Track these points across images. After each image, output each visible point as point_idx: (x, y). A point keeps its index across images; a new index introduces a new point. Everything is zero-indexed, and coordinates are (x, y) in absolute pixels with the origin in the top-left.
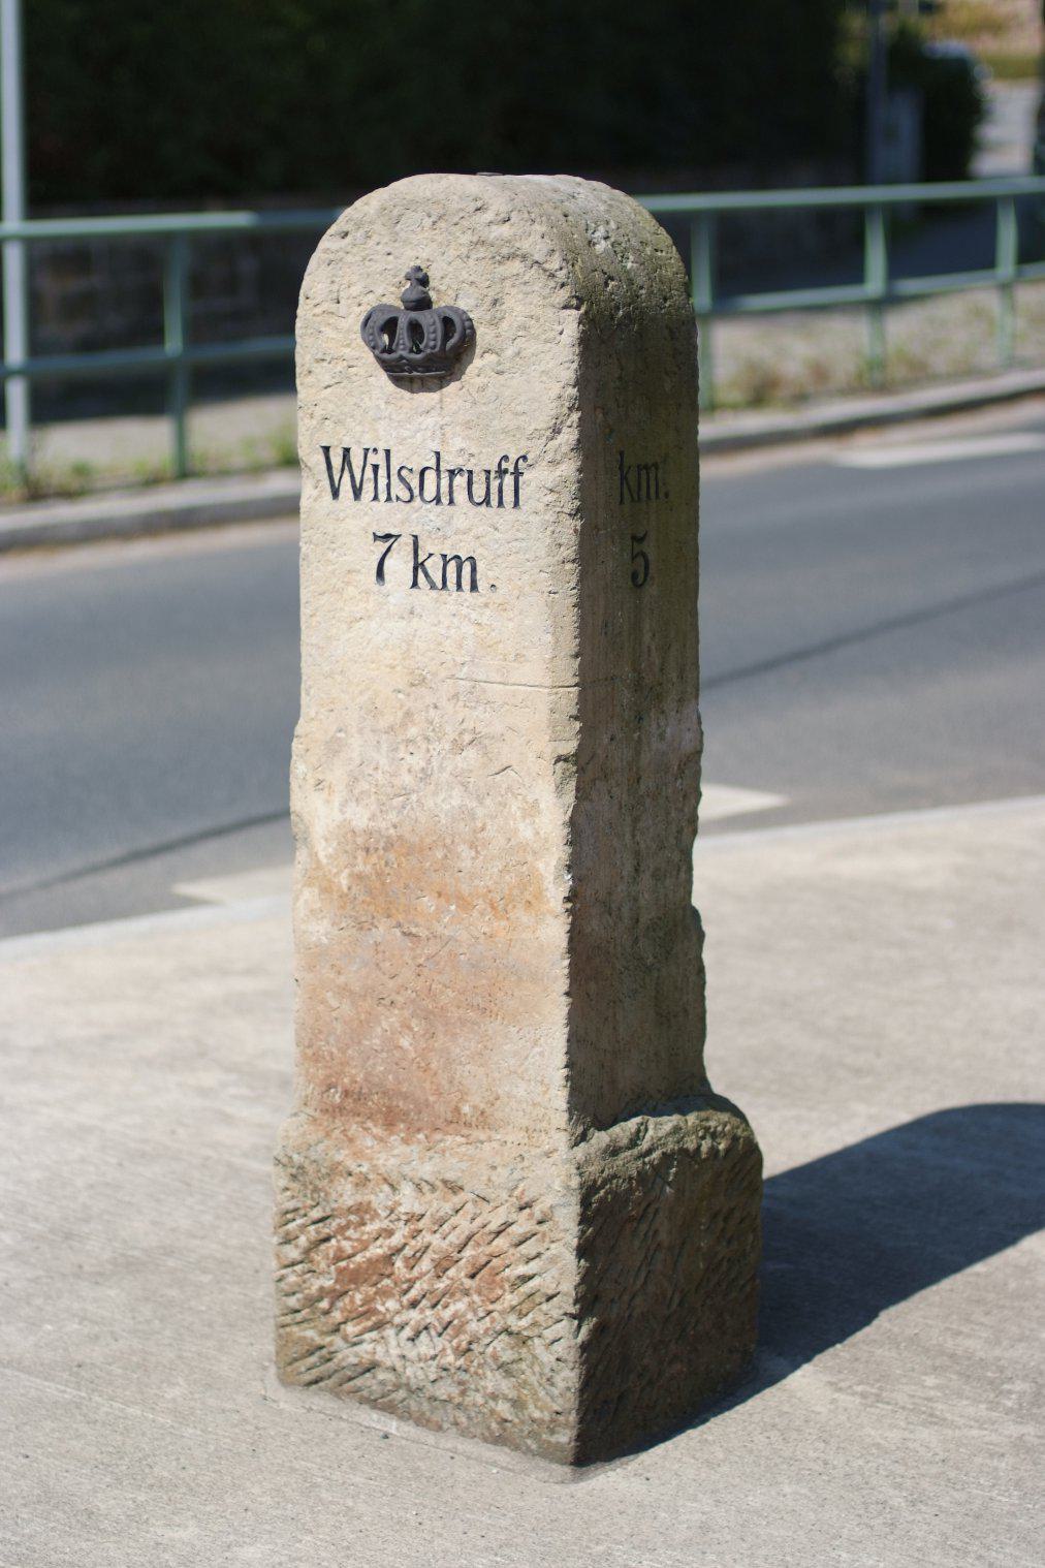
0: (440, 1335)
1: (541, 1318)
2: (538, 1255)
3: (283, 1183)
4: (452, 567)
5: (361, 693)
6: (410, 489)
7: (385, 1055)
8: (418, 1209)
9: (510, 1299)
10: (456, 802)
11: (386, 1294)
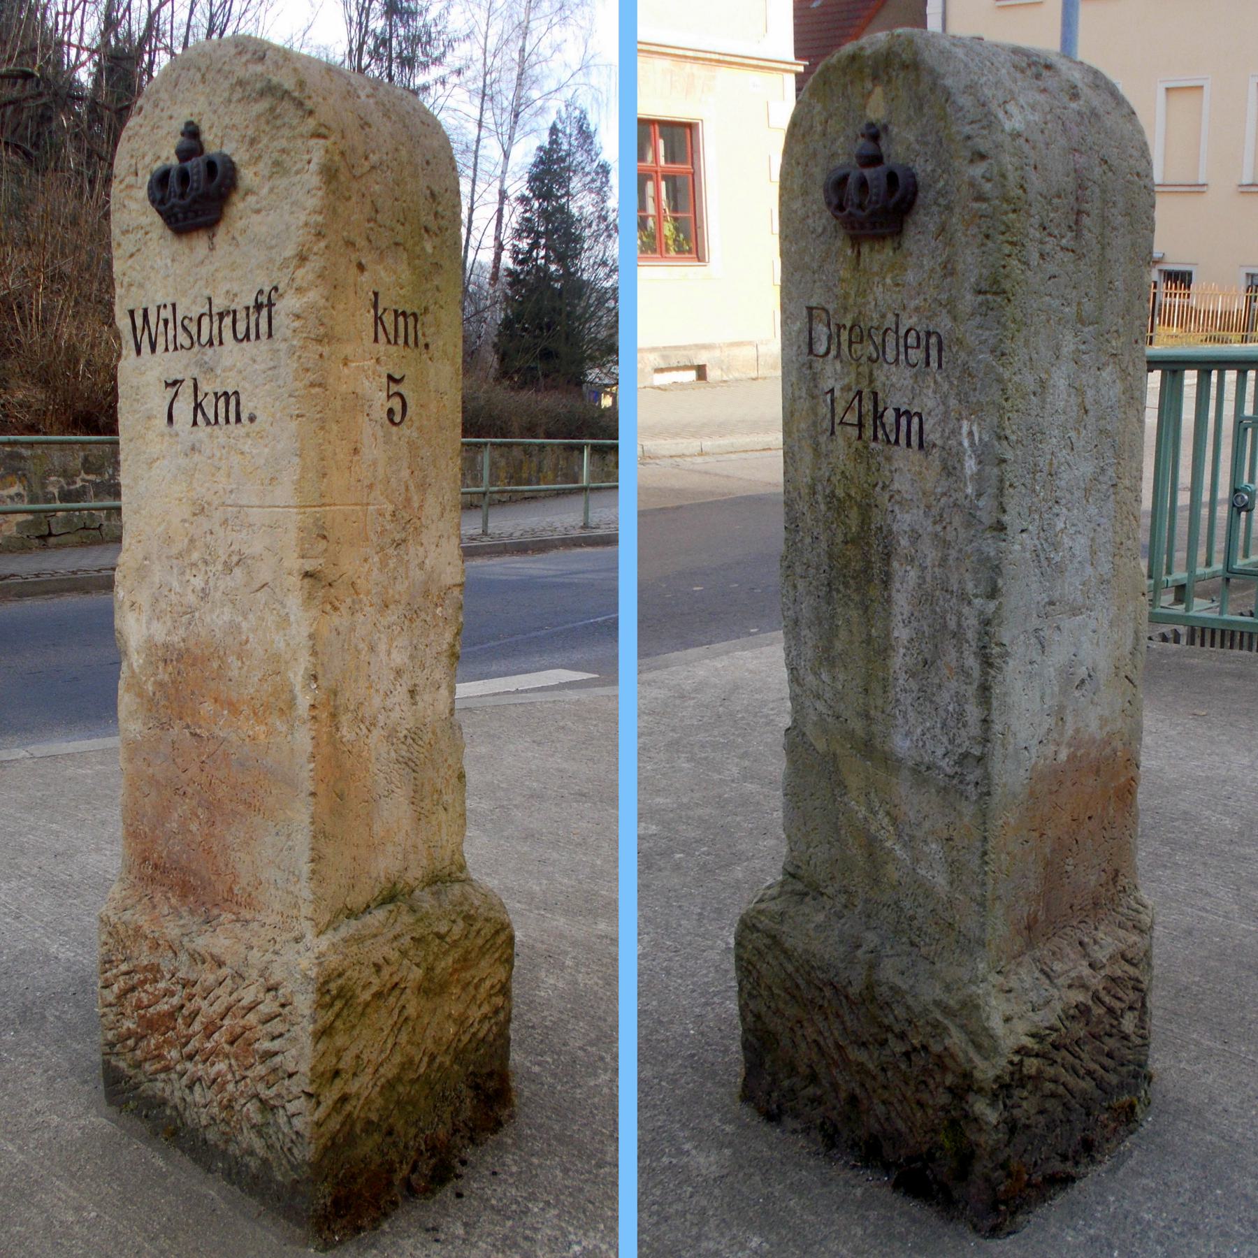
0: (209, 1088)
1: (284, 1092)
2: (281, 1035)
3: (104, 937)
4: (222, 401)
5: (159, 524)
6: (191, 338)
7: (180, 837)
8: (193, 977)
9: (260, 1070)
10: (226, 617)
11: (170, 1043)
